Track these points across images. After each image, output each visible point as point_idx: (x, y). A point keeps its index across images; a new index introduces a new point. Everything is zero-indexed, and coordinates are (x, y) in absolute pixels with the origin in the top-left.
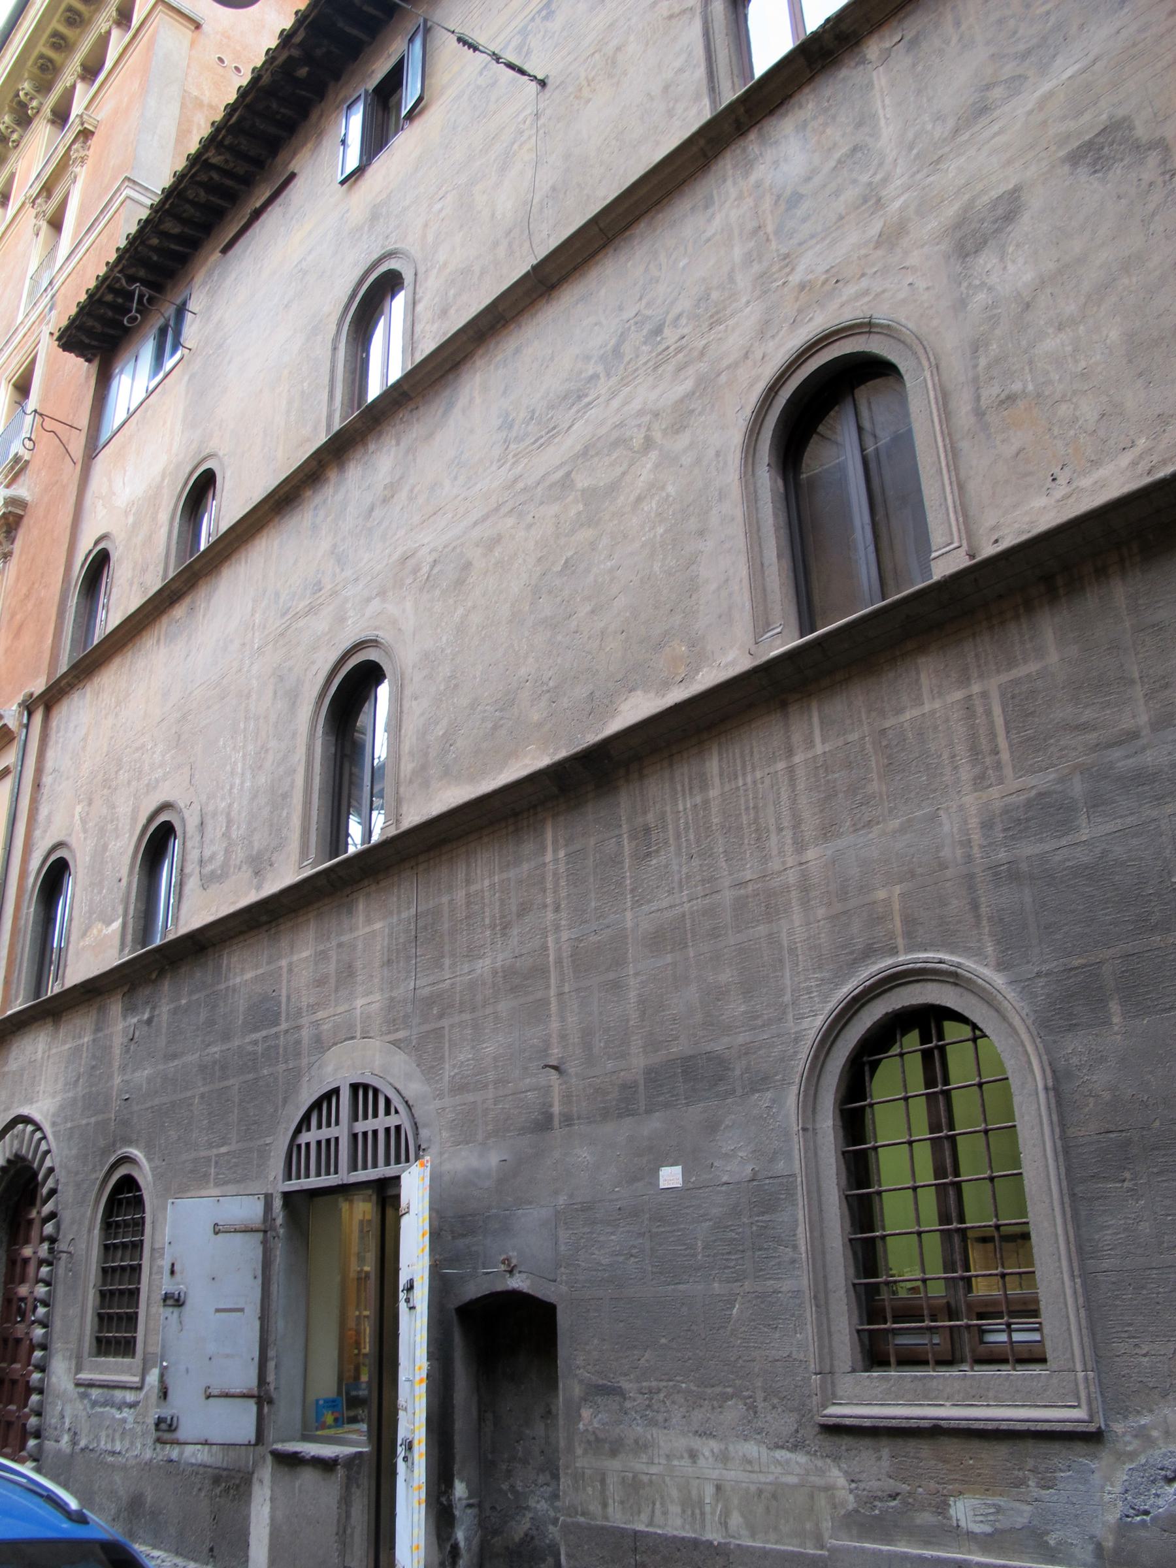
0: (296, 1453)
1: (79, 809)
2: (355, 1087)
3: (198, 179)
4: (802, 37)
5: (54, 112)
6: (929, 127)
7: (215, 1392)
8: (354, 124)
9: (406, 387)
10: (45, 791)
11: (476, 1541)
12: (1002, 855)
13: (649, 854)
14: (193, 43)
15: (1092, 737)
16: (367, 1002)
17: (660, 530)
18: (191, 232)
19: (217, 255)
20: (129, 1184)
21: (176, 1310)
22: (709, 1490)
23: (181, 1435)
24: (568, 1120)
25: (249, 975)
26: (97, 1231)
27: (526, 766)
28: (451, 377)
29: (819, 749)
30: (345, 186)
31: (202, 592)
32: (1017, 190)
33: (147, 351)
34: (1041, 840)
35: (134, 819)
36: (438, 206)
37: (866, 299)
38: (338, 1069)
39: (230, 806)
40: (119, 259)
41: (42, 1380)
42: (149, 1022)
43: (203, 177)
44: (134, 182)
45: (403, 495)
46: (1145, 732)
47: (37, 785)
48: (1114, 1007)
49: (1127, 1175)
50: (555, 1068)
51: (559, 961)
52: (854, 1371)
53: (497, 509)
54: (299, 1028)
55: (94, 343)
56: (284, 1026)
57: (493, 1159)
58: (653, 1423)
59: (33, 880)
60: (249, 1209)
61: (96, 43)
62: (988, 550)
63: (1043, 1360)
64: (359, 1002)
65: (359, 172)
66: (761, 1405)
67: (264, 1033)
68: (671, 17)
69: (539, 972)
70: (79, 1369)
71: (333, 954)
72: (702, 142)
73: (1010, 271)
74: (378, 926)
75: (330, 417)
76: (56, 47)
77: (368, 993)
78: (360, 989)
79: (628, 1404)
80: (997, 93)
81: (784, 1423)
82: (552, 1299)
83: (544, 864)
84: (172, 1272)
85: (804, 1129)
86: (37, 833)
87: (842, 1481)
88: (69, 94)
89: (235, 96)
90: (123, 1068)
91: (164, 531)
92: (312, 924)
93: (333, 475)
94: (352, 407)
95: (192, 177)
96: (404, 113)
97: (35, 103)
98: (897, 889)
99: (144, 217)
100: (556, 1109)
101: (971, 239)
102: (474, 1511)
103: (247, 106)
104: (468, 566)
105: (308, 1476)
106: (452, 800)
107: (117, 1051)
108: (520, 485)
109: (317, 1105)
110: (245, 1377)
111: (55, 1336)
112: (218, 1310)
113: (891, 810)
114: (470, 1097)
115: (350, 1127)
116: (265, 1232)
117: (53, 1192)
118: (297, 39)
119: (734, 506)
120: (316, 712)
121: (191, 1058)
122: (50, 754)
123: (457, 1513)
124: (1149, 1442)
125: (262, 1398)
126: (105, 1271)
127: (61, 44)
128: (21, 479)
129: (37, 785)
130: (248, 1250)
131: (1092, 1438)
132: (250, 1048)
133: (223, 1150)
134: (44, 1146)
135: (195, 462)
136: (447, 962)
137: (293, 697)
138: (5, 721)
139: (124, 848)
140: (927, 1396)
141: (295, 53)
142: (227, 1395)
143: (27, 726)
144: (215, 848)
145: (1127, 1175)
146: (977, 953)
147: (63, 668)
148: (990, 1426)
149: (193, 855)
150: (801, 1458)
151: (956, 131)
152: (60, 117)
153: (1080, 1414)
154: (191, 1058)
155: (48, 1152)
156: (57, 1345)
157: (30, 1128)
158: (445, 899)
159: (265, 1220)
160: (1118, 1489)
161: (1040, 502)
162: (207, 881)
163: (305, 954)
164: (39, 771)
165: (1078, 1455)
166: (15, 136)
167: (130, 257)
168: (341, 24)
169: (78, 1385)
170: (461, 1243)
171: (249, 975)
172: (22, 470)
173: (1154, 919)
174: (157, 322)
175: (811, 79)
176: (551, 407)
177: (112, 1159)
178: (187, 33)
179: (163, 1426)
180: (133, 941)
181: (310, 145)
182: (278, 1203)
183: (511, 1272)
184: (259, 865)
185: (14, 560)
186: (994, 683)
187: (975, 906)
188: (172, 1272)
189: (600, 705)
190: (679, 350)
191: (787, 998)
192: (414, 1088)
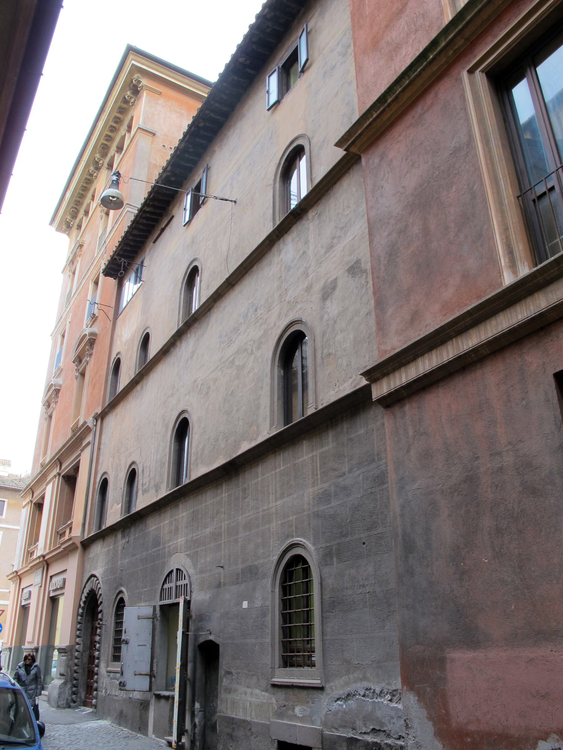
0: (159, 694)
1: (111, 459)
2: (177, 569)
5: (108, 165)
6: (320, 249)
7: (137, 673)
8: (273, 81)
10: (101, 451)
11: (202, 723)
12: (316, 509)
13: (245, 498)
14: (152, 142)
15: (336, 473)
16: (181, 540)
17: (253, 384)
18: (192, 158)
19: (152, 244)
20: (122, 601)
21: (126, 645)
22: (248, 704)
23: (127, 687)
24: (224, 584)
25: (154, 528)
26: (113, 617)
28: (208, 313)
29: (282, 468)
30: (271, 111)
31: (144, 382)
32: (336, 279)
33: (133, 276)
34: (324, 505)
35: (126, 466)
36: (208, 243)
37: (302, 311)
38: (173, 565)
39: (150, 465)
40: (120, 245)
41: (97, 670)
42: (128, 542)
43: (144, 215)
44: (130, 205)
45: (195, 357)
46: (347, 473)
47: (99, 449)
48: (335, 559)
49: (334, 611)
50: (222, 567)
51: (224, 531)
52: (279, 667)
53: (217, 368)
54: (165, 548)
56: (161, 547)
57: (208, 596)
58: (238, 683)
59: (98, 486)
60: (149, 611)
61: (121, 139)
62: (320, 407)
63: (314, 666)
64: (180, 540)
65: (278, 103)
66: (260, 678)
67: (156, 549)
68: (267, 186)
69: (220, 534)
70: (107, 666)
71: (174, 522)
72: (268, 242)
73: (333, 308)
74: (184, 514)
76: (116, 122)
77: (182, 537)
78: (180, 536)
79: (233, 677)
80: (335, 241)
81: (264, 683)
82: (218, 643)
83: (222, 498)
84: (125, 632)
85: (272, 592)
86: (99, 467)
87: (275, 702)
88: (113, 158)
89: (187, 128)
90: (121, 558)
91: (135, 354)
93: (178, 344)
94: (186, 317)
96: (201, 202)
97: (101, 162)
98: (295, 517)
99: (126, 230)
100: (222, 581)
101: (327, 293)
102: (203, 713)
103: (187, 142)
104: (209, 388)
105: (163, 701)
107: (120, 552)
108: (223, 360)
109: (168, 575)
110: (146, 669)
111: (101, 655)
112: (139, 645)
113: (295, 491)
114: (203, 575)
115: (176, 583)
116: (153, 619)
117: (101, 603)
118: (169, 169)
119: (268, 380)
120: (172, 434)
121: (138, 556)
122: (103, 437)
123: (196, 713)
124: (332, 690)
125: (151, 675)
126: (116, 631)
127: (109, 139)
128: (96, 323)
129: (99, 449)
130: (148, 624)
131: (322, 689)
132: (153, 554)
133: (146, 589)
134: (99, 586)
136: (200, 528)
137: (167, 427)
138: (88, 424)
139: (123, 476)
140: (292, 676)
141: (168, 174)
142: (141, 674)
143: (96, 426)
144: (146, 480)
145: (334, 611)
146: (308, 539)
147: (107, 403)
148: (302, 685)
149: (140, 482)
150: (267, 694)
151: (326, 253)
152: (110, 166)
153: (319, 682)
154: (138, 556)
155: (100, 588)
156: (102, 658)
157: (95, 579)
158: (200, 506)
159: (153, 615)
160: (326, 704)
161: (332, 393)
162: (145, 491)
163: (167, 522)
164: (100, 443)
165: (316, 694)
166: (95, 174)
168: (182, 163)
169: (107, 672)
170: (200, 624)
171: (154, 528)
172: (96, 319)
173: (344, 533)
174: (135, 267)
175: (296, 223)
176: (231, 332)
177: (118, 591)
178: (149, 138)
179: (122, 685)
180: (125, 512)
181: (178, 205)
182: (158, 609)
183: (210, 634)
184: (157, 488)
185: (93, 356)
186: (317, 452)
187: (309, 524)
188: (125, 632)
189: (237, 445)
190: (261, 318)
191: (271, 549)
192: (191, 571)
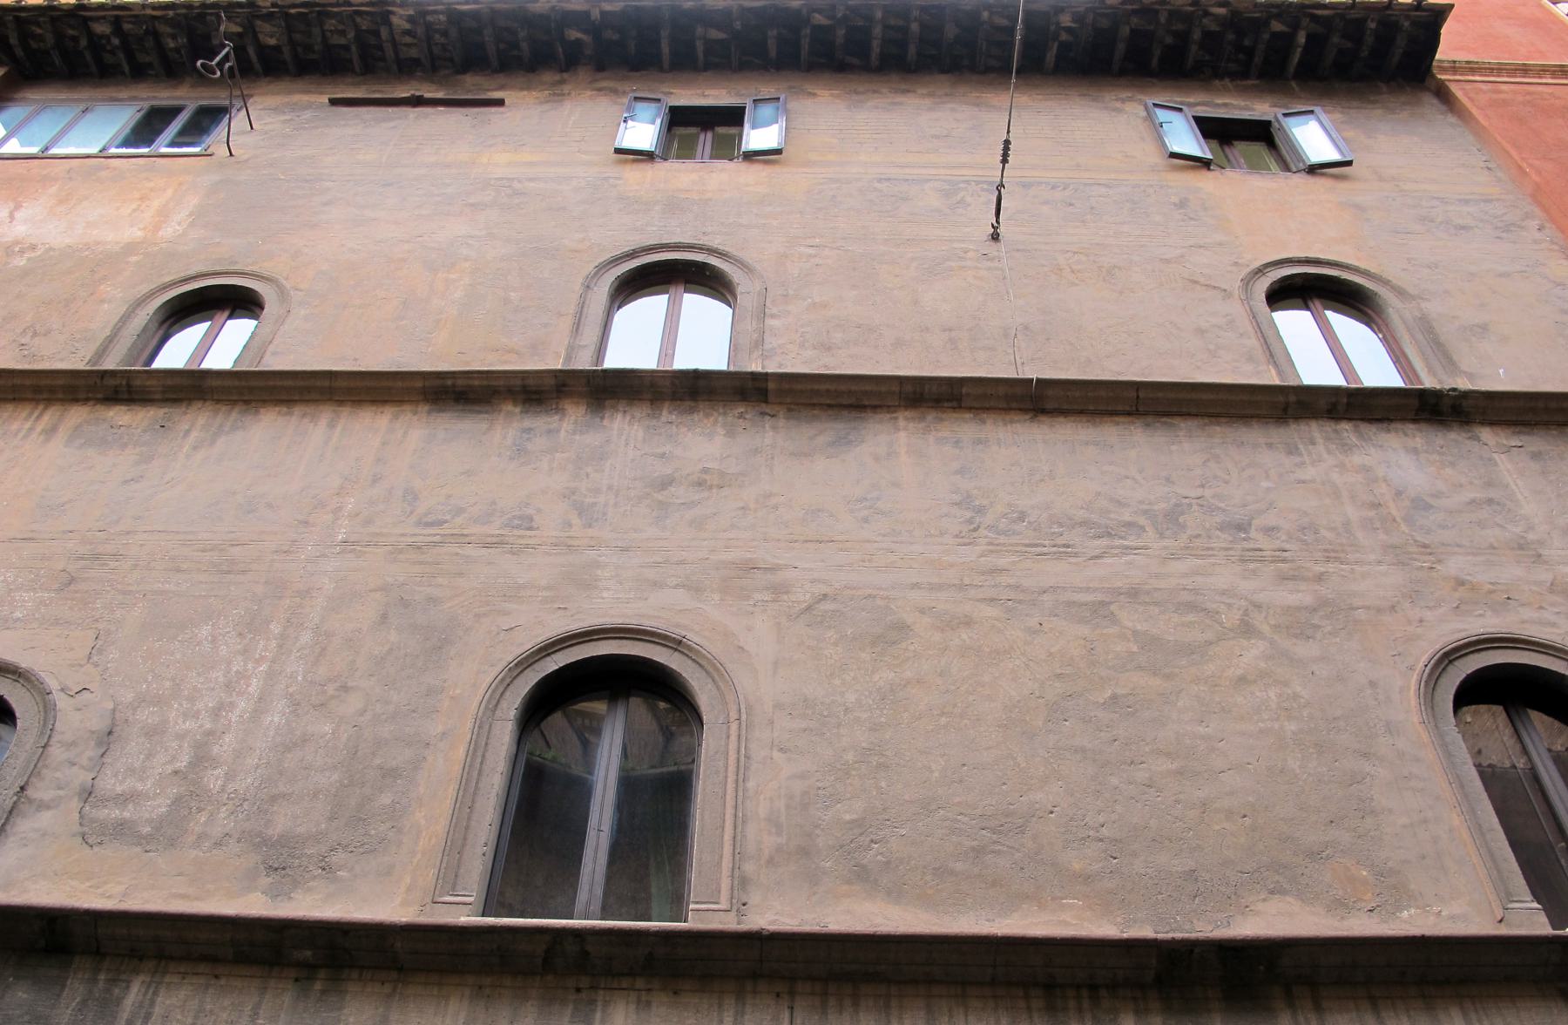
3: (358, 20)
4: (194, 367)
9: (771, 385)
27: (1066, 924)
55: (19, 52)
72: (1292, 398)
75: (110, 340)
92: (569, 1011)
95: (356, 12)
106: (879, 920)
135: (218, 268)
167: (185, 16)
174: (164, 96)
